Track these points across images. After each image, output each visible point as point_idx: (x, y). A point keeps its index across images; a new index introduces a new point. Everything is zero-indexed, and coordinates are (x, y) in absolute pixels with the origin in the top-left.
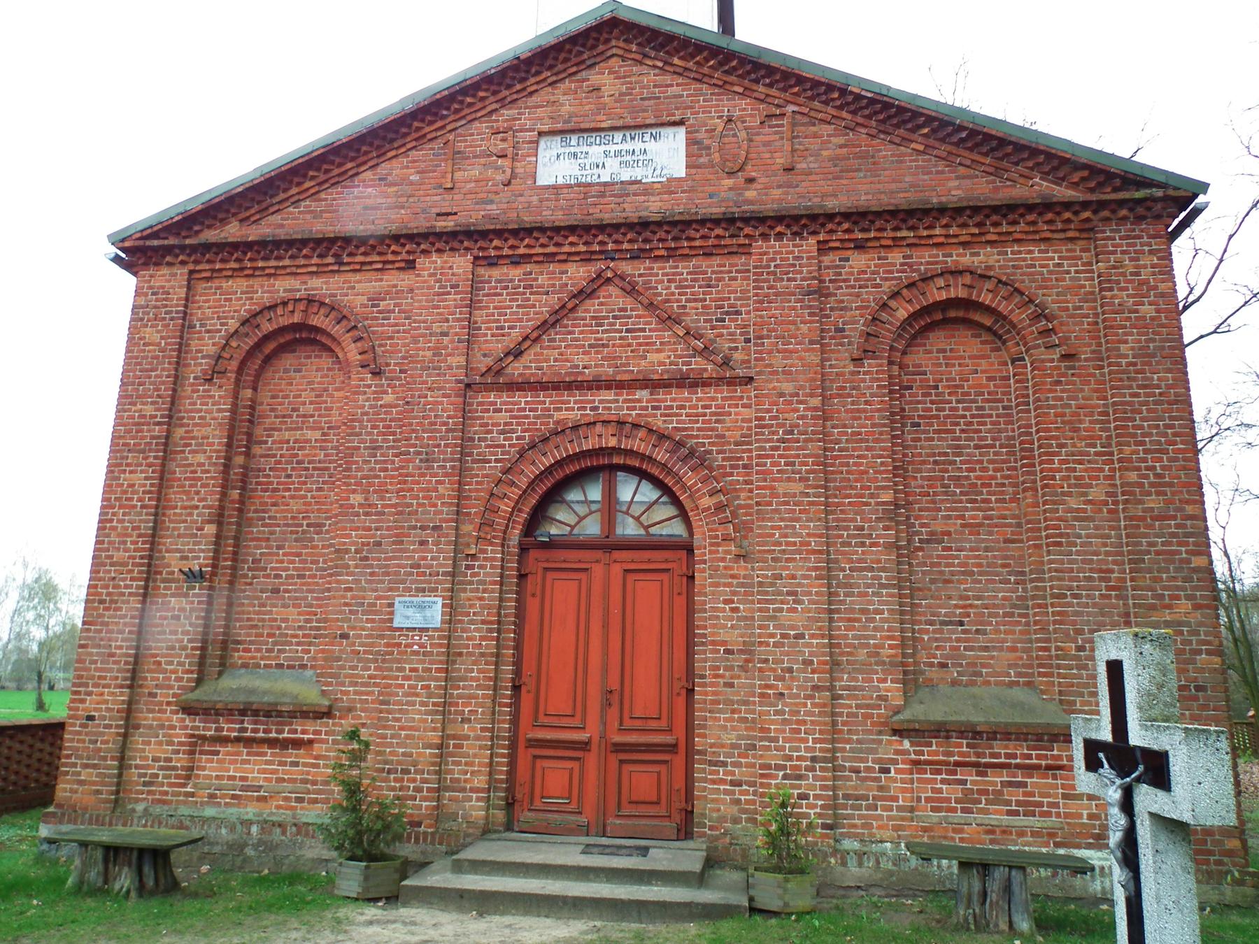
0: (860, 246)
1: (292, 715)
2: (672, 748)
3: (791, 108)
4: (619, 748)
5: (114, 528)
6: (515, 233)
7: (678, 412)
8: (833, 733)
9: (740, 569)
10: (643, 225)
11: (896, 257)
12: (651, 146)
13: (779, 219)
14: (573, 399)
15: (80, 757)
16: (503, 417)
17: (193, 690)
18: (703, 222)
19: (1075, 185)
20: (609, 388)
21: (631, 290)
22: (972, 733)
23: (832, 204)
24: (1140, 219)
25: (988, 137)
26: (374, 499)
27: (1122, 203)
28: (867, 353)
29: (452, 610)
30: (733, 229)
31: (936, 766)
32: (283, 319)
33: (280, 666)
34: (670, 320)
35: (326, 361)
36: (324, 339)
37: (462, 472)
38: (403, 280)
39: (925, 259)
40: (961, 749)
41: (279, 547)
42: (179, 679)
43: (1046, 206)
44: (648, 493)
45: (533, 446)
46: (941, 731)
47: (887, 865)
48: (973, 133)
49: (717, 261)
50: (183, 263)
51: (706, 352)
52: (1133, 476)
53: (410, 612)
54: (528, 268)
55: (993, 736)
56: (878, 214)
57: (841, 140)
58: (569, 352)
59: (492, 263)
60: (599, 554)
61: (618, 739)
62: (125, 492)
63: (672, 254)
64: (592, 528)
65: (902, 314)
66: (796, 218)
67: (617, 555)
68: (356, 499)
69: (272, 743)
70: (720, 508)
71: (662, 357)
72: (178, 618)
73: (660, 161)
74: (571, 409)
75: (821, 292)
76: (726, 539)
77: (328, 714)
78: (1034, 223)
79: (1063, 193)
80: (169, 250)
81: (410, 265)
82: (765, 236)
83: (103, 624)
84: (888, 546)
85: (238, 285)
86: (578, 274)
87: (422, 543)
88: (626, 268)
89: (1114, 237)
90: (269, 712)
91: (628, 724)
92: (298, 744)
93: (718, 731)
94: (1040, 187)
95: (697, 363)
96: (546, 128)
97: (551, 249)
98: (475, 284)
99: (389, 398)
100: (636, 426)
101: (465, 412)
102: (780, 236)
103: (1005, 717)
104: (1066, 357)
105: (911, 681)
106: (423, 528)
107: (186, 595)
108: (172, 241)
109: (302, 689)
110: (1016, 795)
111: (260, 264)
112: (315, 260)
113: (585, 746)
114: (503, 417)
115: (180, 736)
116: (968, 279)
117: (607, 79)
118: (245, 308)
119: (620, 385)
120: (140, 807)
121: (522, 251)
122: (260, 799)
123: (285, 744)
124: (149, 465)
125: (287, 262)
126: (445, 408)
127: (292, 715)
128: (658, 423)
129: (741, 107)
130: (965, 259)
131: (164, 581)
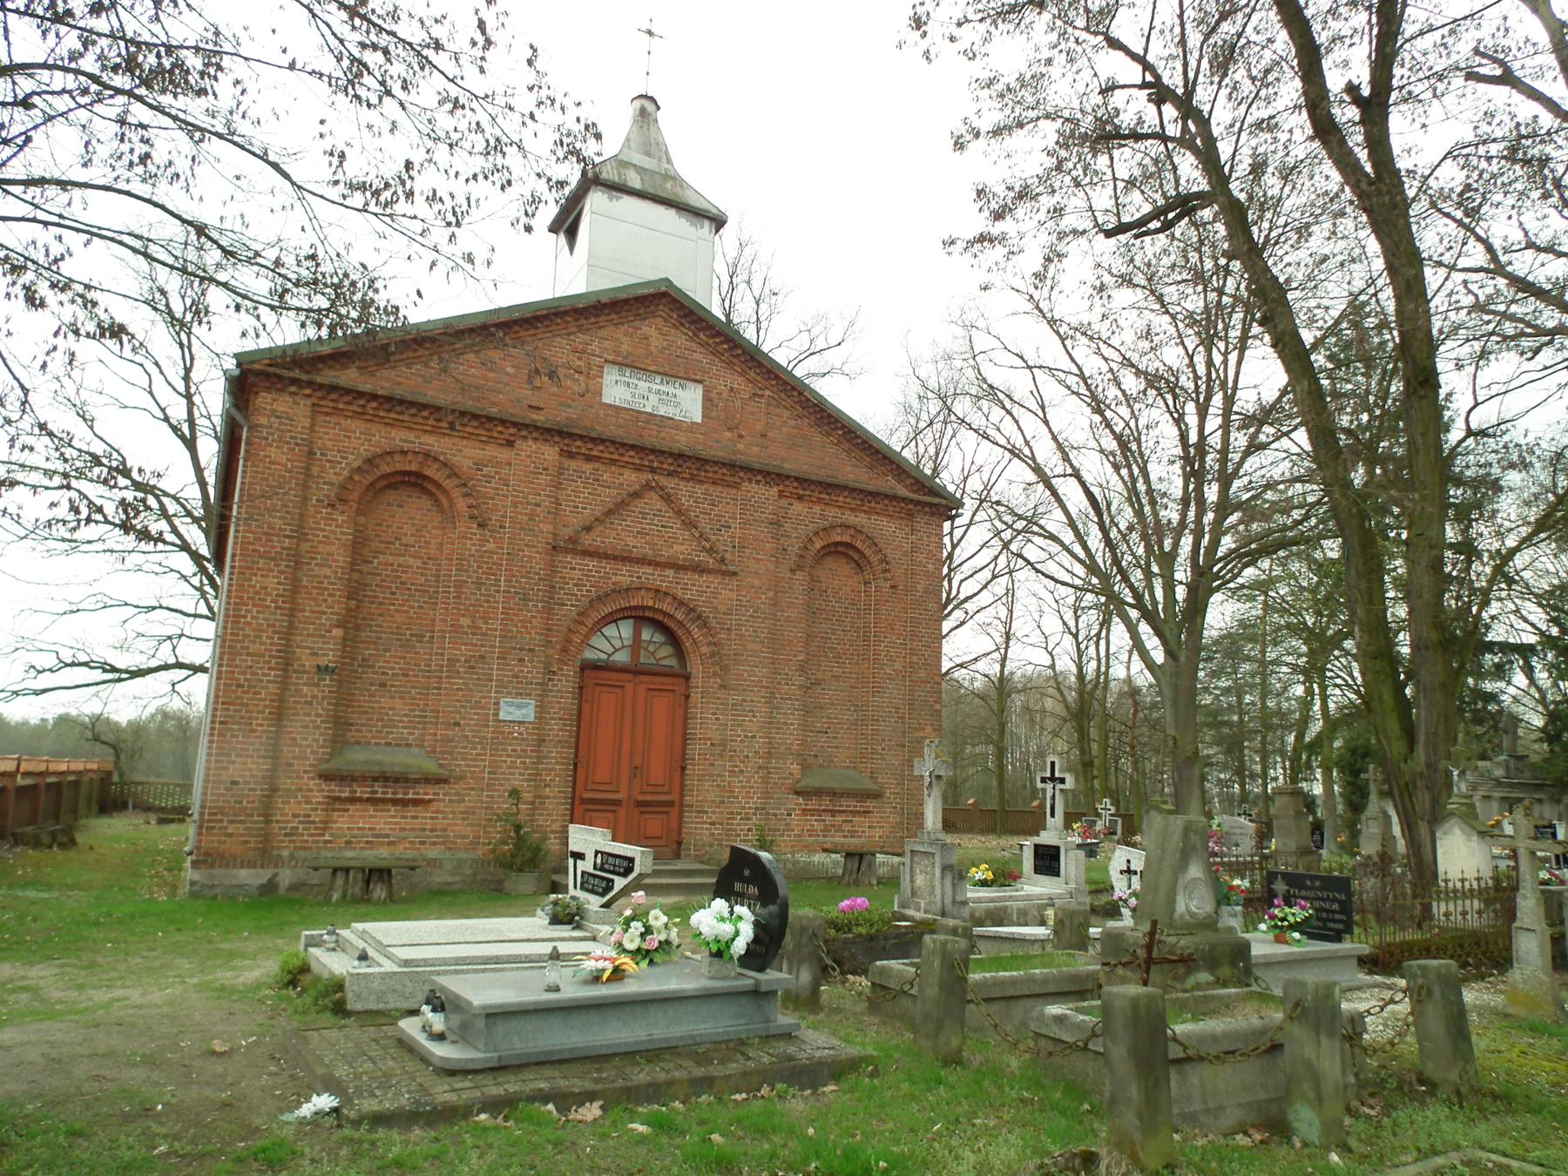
0: (800, 498)
1: (417, 781)
2: (671, 804)
3: (767, 393)
4: (639, 804)
5: (249, 624)
6: (593, 440)
7: (693, 588)
8: (767, 795)
9: (722, 694)
10: (679, 456)
11: (817, 509)
12: (679, 392)
13: (760, 472)
14: (625, 569)
15: (227, 815)
16: (577, 574)
17: (327, 761)
18: (716, 463)
19: (906, 486)
20: (649, 564)
21: (667, 499)
22: (833, 794)
23: (789, 467)
24: (933, 514)
25: (871, 446)
26: (480, 623)
27: (928, 504)
28: (800, 567)
29: (541, 709)
30: (734, 471)
31: (813, 812)
32: (401, 464)
33: (388, 744)
34: (690, 525)
35: (426, 502)
36: (430, 487)
37: (549, 611)
38: (504, 454)
39: (832, 512)
40: (826, 802)
41: (386, 650)
42: (314, 753)
43: (894, 498)
44: (659, 638)
45: (599, 598)
46: (818, 792)
47: (789, 866)
48: (864, 442)
49: (719, 488)
50: (309, 396)
51: (711, 551)
52: (915, 659)
53: (511, 709)
54: (597, 465)
55: (842, 795)
56: (813, 482)
57: (792, 423)
58: (623, 535)
59: (571, 456)
60: (631, 677)
61: (640, 798)
62: (258, 593)
63: (693, 478)
64: (622, 657)
65: (818, 546)
66: (769, 474)
67: (643, 678)
68: (465, 621)
69: (395, 802)
70: (713, 655)
71: (683, 548)
72: (310, 703)
73: (686, 405)
74: (624, 576)
75: (776, 524)
76: (715, 674)
77: (445, 781)
78: (363, 406)
79: (902, 491)
80: (294, 381)
81: (510, 444)
82: (750, 481)
83: (242, 705)
84: (801, 687)
85: (357, 426)
86: (631, 479)
87: (521, 660)
88: (664, 481)
89: (921, 521)
90: (401, 779)
91: (591, 786)
92: (416, 802)
93: (701, 791)
94: (889, 484)
95: (704, 557)
96: (611, 358)
97: (616, 457)
98: (561, 469)
99: (491, 546)
100: (666, 594)
101: (551, 566)
102: (758, 482)
103: (849, 785)
104: (893, 587)
105: (805, 767)
106: (521, 649)
107: (318, 685)
108: (296, 374)
109: (415, 760)
110: (847, 827)
111: (382, 414)
112: (431, 422)
113: (618, 803)
114: (577, 574)
115: (318, 797)
116: (852, 532)
117: (656, 333)
118: (365, 450)
119: (658, 564)
120: (285, 853)
121: (595, 453)
122: (390, 843)
123: (404, 803)
124: (281, 572)
125: (406, 417)
126: (538, 565)
127: (417, 781)
128: (679, 593)
129: (738, 382)
130: (850, 518)
131: (296, 671)
